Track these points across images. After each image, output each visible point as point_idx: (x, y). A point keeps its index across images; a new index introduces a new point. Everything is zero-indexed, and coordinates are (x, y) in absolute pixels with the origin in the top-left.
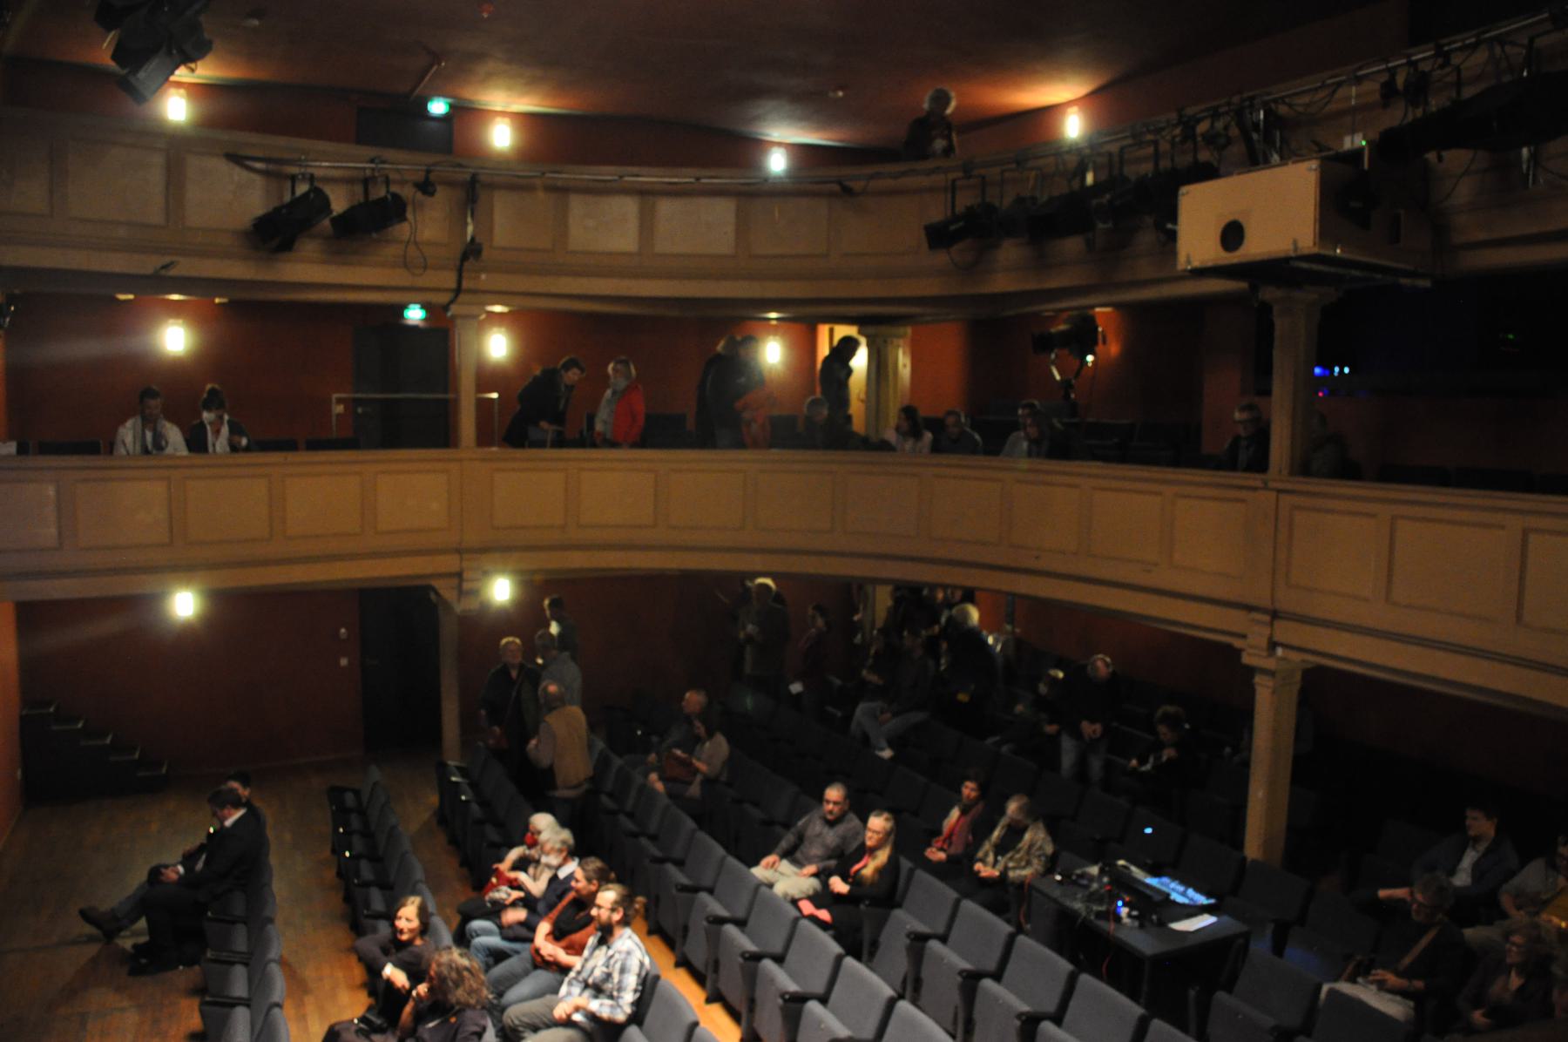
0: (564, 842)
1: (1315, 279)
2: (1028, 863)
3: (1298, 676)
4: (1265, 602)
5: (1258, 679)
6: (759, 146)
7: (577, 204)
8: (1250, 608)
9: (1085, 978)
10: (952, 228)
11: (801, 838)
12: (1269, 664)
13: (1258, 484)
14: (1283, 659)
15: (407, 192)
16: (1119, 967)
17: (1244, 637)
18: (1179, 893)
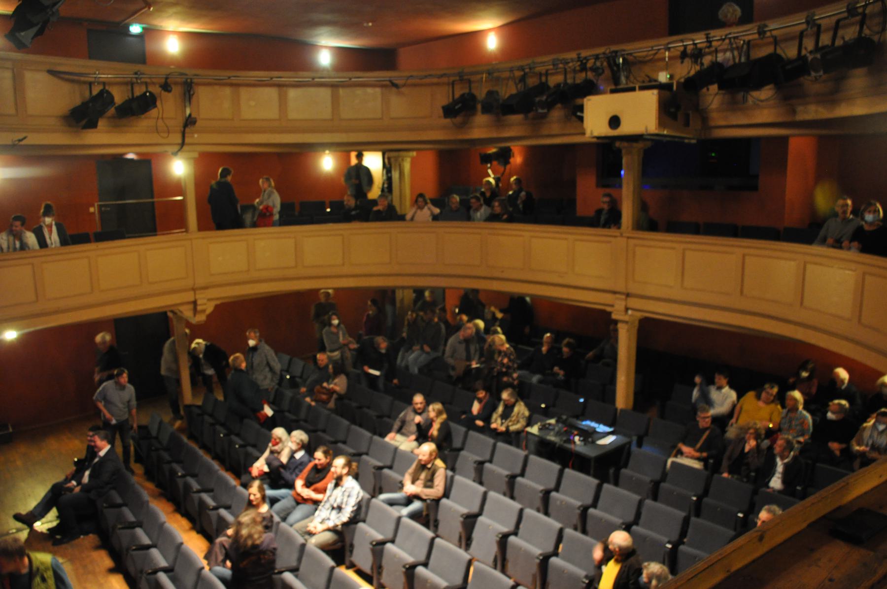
0: (302, 441)
1: (648, 140)
2: (518, 422)
3: (637, 323)
4: (623, 290)
5: (620, 325)
6: (313, 48)
7: (244, 92)
8: (615, 293)
9: (568, 471)
10: (457, 107)
11: (403, 423)
12: (626, 318)
13: (618, 234)
14: (631, 315)
15: (156, 90)
16: (581, 463)
17: (612, 306)
18: (602, 428)
